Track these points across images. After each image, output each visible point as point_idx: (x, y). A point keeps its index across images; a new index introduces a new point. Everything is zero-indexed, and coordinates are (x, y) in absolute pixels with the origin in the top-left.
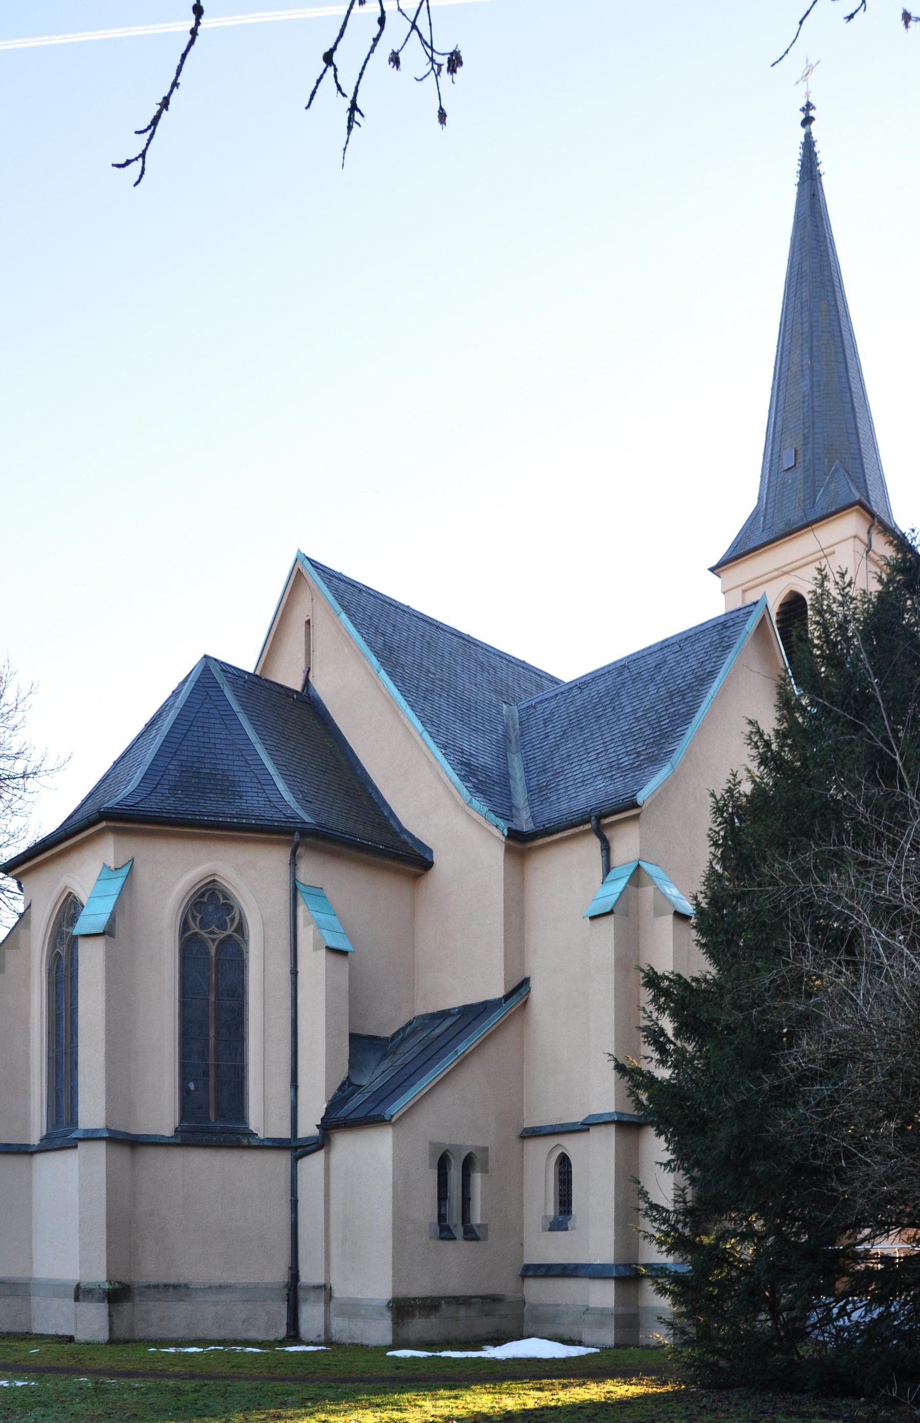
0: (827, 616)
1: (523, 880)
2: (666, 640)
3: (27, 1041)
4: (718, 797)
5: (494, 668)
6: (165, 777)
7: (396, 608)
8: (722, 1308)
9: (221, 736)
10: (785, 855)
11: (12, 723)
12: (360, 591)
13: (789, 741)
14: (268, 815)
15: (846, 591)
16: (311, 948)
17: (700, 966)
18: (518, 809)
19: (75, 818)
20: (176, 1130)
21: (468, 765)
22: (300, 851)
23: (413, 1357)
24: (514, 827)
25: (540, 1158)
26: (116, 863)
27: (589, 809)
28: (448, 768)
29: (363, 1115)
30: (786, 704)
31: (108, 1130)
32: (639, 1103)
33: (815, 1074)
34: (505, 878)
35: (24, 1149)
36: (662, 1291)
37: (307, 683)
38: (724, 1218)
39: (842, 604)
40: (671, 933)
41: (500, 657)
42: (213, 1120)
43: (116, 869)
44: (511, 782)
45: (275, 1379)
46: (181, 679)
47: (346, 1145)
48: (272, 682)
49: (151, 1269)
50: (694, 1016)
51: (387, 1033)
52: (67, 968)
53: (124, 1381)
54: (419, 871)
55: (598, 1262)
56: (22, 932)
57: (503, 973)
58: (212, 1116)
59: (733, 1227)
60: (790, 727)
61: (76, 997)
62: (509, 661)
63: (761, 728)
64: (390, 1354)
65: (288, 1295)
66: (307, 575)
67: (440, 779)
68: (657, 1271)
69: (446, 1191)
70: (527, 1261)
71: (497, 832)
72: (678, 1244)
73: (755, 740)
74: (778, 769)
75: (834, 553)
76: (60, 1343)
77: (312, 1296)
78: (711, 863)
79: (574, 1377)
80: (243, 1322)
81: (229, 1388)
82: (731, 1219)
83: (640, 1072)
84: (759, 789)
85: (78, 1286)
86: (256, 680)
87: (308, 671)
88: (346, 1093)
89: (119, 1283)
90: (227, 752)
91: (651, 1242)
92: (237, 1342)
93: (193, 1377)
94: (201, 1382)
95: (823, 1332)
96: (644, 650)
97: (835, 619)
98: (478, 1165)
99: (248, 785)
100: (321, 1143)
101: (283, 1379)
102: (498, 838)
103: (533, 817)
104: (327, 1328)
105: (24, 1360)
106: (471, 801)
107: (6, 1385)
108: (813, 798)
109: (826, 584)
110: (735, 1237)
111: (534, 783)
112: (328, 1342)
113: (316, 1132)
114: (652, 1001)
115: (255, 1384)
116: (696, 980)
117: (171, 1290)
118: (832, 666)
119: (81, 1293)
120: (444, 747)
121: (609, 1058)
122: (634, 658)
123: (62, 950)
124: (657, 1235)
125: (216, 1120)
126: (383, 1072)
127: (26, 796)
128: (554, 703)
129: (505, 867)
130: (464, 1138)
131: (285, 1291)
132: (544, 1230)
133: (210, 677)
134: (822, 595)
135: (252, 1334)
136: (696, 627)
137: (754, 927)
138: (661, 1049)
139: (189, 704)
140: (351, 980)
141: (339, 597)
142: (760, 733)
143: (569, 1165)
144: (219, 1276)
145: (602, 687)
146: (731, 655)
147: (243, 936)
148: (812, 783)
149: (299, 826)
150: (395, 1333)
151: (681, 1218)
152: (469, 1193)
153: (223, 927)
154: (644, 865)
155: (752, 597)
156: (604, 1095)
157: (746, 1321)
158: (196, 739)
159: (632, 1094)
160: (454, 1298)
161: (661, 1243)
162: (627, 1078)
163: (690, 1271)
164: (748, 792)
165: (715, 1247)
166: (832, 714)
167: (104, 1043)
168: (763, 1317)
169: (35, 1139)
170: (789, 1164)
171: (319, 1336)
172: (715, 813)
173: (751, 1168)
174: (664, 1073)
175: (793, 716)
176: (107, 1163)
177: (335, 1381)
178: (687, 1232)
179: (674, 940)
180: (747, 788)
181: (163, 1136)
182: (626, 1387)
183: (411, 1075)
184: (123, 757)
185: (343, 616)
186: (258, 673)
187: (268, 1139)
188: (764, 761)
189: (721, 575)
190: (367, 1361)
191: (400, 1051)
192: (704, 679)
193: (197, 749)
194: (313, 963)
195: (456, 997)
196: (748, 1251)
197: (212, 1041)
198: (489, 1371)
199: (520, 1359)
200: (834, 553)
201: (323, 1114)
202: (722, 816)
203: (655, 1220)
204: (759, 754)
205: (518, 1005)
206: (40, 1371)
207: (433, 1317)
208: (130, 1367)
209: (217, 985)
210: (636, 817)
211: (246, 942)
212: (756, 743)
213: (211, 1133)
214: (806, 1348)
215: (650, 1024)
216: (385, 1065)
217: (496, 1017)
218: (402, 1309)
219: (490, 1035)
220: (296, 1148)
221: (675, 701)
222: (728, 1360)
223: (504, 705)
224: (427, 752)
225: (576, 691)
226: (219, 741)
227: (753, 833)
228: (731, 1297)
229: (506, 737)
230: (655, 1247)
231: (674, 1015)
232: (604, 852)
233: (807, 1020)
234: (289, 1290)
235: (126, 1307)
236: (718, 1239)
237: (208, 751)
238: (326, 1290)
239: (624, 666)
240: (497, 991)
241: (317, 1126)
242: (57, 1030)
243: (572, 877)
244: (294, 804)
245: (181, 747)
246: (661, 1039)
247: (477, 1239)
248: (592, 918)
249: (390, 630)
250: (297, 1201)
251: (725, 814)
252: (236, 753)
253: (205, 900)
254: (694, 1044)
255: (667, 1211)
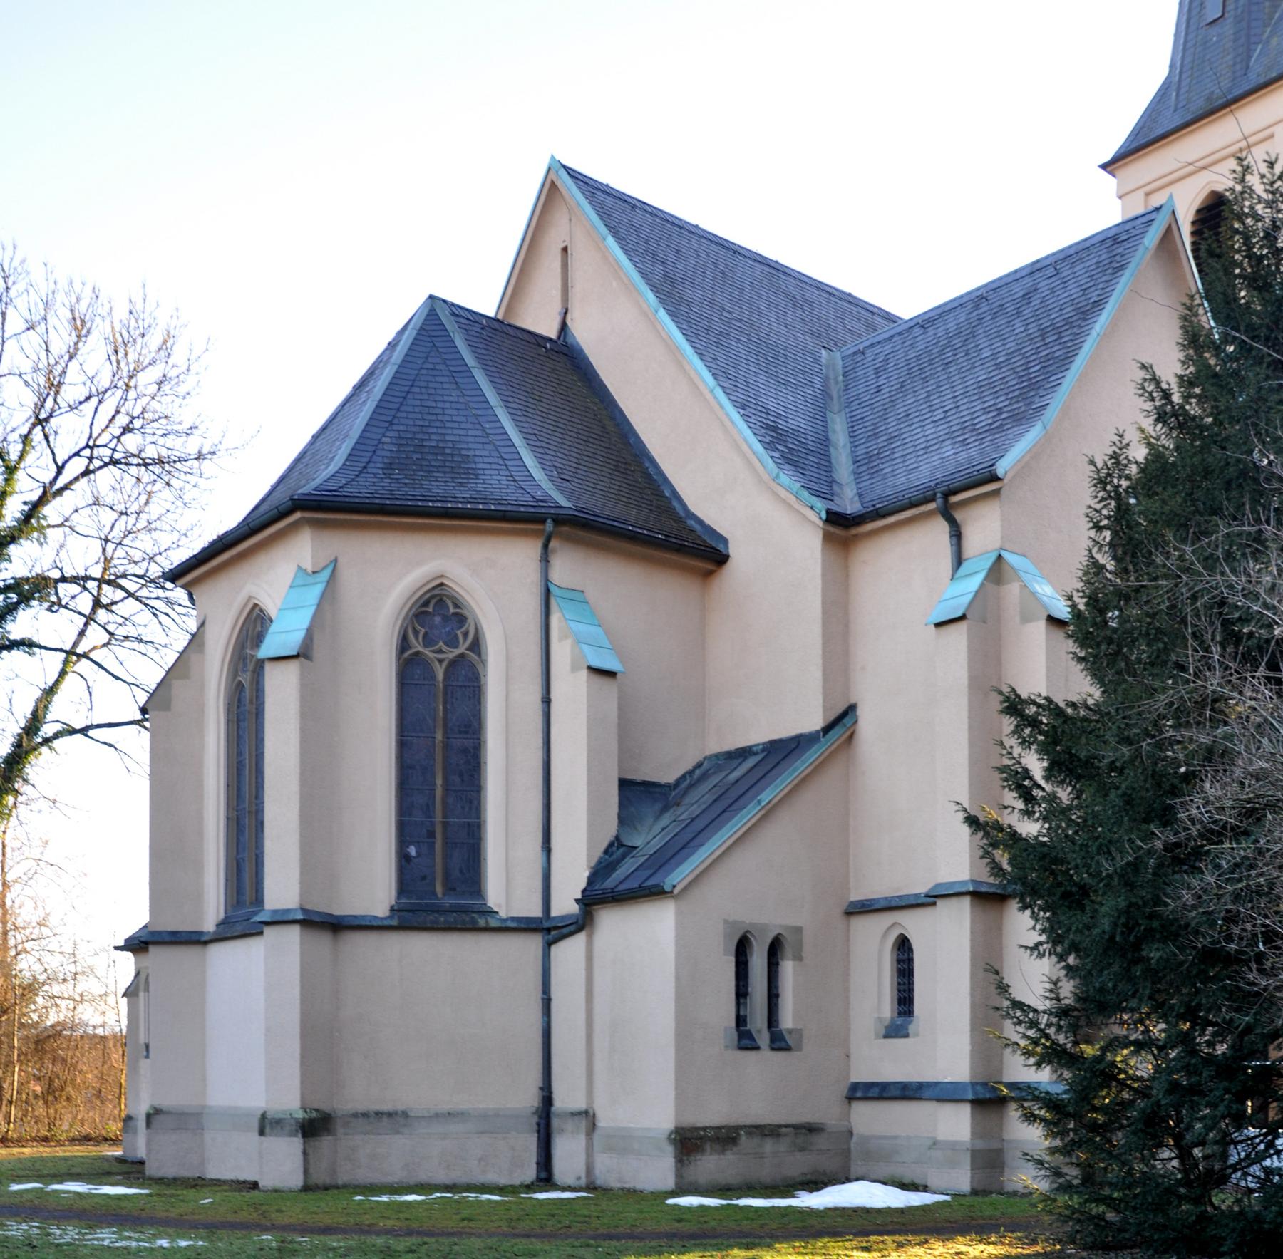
0: (1249, 221)
1: (847, 576)
2: (1038, 261)
3: (200, 796)
4: (1100, 465)
5: (810, 303)
6: (379, 453)
7: (681, 228)
8: (1109, 1141)
9: (452, 399)
10: (1184, 540)
11: (182, 390)
12: (633, 207)
13: (1197, 390)
14: (512, 498)
15: (1276, 186)
16: (568, 668)
17: (1080, 688)
18: (841, 485)
19: (262, 509)
20: (392, 909)
21: (774, 429)
22: (554, 544)
23: (702, 1207)
24: (835, 509)
25: (873, 939)
26: (313, 565)
27: (932, 484)
28: (748, 433)
29: (636, 885)
30: (1194, 340)
31: (303, 910)
32: (996, 869)
33: (1224, 827)
34: (823, 575)
35: (195, 937)
36: (1030, 1118)
37: (564, 327)
38: (1112, 1020)
39: (1269, 204)
40: (1044, 644)
41: (818, 288)
42: (440, 895)
43: (314, 572)
44: (832, 449)
45: (517, 1236)
46: (400, 327)
47: (614, 925)
48: (518, 328)
49: (357, 1094)
50: (1070, 753)
51: (669, 777)
52: (251, 702)
53: (318, 1240)
54: (710, 567)
55: (949, 1080)
56: (194, 658)
57: (821, 697)
58: (439, 889)
59: (1125, 1032)
60: (1198, 371)
61: (263, 739)
62: (831, 294)
63: (1158, 373)
64: (670, 1201)
65: (538, 1124)
66: (562, 189)
67: (737, 448)
68: (1024, 1092)
69: (746, 986)
70: (856, 1077)
71: (811, 515)
72: (1054, 1055)
73: (1149, 389)
74: (1181, 426)
75: (1272, 136)
76: (240, 1191)
77: (569, 1125)
78: (1090, 551)
79: (914, 1233)
80: (480, 1160)
81: (456, 1248)
82: (1123, 1023)
83: (999, 827)
84: (1156, 456)
85: (263, 1116)
86: (496, 325)
87: (566, 313)
88: (614, 857)
89: (317, 1110)
90: (458, 419)
91: (1014, 1051)
92: (470, 1188)
93: (410, 1233)
94: (419, 1240)
95: (1245, 1174)
96: (1008, 275)
97: (1260, 224)
98: (788, 950)
99: (486, 460)
100: (582, 923)
101: (528, 1236)
102: (813, 523)
103: (860, 495)
104: (589, 1169)
105: (193, 1213)
106: (777, 476)
107: (166, 1245)
108: (1228, 464)
109: (1248, 178)
110: (1126, 1047)
111: (861, 451)
112: (591, 1187)
113: (574, 909)
114: (1014, 733)
115: (490, 1242)
116: (1073, 705)
117: (385, 1119)
118: (1255, 289)
119: (266, 1125)
120: (742, 406)
121: (958, 807)
122: (994, 286)
123: (245, 678)
124: (1023, 1043)
125: (444, 894)
126: (663, 829)
127: (202, 482)
128: (888, 348)
129: (823, 561)
130: (769, 917)
131: (535, 1119)
132: (877, 1037)
133: (437, 326)
134: (1242, 193)
135: (492, 1177)
136: (1078, 243)
137: (1148, 634)
138: (1027, 796)
139: (409, 359)
140: (621, 708)
141: (604, 215)
142: (1156, 381)
143: (911, 950)
144: (446, 1102)
145: (952, 325)
146: (1125, 279)
147: (479, 655)
148: (1229, 446)
149: (552, 511)
150: (679, 1175)
151: (1054, 1020)
152: (777, 988)
153: (453, 643)
154: (1005, 555)
155: (1156, 200)
156: (957, 859)
157: (1142, 1160)
158: (418, 403)
159: (986, 854)
160: (757, 1127)
161: (1027, 1054)
162: (981, 834)
163: (1065, 1092)
164: (1141, 459)
165: (1099, 1059)
166: (1254, 353)
167: (298, 797)
168: (1166, 1154)
169: (209, 924)
170: (1195, 948)
171: (579, 1178)
172: (1095, 485)
173: (1144, 953)
174: (1030, 828)
175: (1201, 357)
176: (302, 954)
177: (594, 1238)
178: (1061, 1039)
179: (1047, 653)
180: (1139, 453)
181: (376, 917)
182: (982, 1247)
183: (700, 833)
184: (324, 428)
185: (611, 241)
186: (500, 317)
187: (513, 919)
188: (1161, 417)
189: (1117, 173)
190: (641, 1212)
191: (687, 800)
192: (1088, 311)
193: (419, 416)
194: (572, 689)
195: (761, 729)
196: (1143, 1066)
197: (439, 792)
198: (800, 1224)
199: (844, 1208)
200: (1272, 136)
201: (583, 884)
202: (1104, 490)
203: (1020, 1023)
204: (1155, 408)
205: (842, 739)
206: (212, 1228)
207: (729, 1152)
208: (327, 1220)
209: (445, 719)
210: (996, 493)
211: (484, 663)
212: (1150, 393)
213: (438, 911)
214: (1222, 1196)
215: (1010, 762)
216: (665, 820)
217: (812, 756)
218: (687, 1142)
219: (804, 780)
220: (549, 930)
221: (1048, 340)
222: (1118, 1212)
223: (823, 351)
224: (720, 413)
225: (917, 331)
226: (448, 405)
227: (1160, 509)
228: (1122, 1127)
229: (825, 392)
230: (1019, 1059)
231: (1044, 750)
232: (955, 539)
233: (1217, 757)
234: (540, 1117)
235: (325, 1142)
236: (1104, 1050)
237: (434, 417)
238: (588, 1117)
239: (981, 297)
240: (813, 721)
241: (577, 901)
242: (239, 782)
243: (912, 573)
244: (546, 485)
245: (399, 414)
246: (1026, 783)
247: (787, 1048)
248: (938, 625)
249: (672, 257)
250: (549, 1000)
251: (1108, 487)
252: (470, 419)
253: (430, 609)
254: (1070, 789)
255: (1035, 1011)
